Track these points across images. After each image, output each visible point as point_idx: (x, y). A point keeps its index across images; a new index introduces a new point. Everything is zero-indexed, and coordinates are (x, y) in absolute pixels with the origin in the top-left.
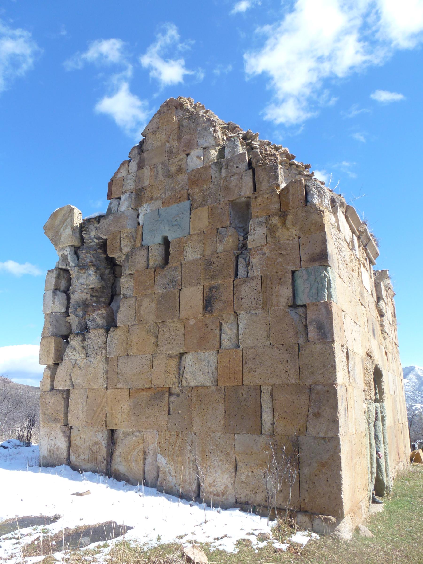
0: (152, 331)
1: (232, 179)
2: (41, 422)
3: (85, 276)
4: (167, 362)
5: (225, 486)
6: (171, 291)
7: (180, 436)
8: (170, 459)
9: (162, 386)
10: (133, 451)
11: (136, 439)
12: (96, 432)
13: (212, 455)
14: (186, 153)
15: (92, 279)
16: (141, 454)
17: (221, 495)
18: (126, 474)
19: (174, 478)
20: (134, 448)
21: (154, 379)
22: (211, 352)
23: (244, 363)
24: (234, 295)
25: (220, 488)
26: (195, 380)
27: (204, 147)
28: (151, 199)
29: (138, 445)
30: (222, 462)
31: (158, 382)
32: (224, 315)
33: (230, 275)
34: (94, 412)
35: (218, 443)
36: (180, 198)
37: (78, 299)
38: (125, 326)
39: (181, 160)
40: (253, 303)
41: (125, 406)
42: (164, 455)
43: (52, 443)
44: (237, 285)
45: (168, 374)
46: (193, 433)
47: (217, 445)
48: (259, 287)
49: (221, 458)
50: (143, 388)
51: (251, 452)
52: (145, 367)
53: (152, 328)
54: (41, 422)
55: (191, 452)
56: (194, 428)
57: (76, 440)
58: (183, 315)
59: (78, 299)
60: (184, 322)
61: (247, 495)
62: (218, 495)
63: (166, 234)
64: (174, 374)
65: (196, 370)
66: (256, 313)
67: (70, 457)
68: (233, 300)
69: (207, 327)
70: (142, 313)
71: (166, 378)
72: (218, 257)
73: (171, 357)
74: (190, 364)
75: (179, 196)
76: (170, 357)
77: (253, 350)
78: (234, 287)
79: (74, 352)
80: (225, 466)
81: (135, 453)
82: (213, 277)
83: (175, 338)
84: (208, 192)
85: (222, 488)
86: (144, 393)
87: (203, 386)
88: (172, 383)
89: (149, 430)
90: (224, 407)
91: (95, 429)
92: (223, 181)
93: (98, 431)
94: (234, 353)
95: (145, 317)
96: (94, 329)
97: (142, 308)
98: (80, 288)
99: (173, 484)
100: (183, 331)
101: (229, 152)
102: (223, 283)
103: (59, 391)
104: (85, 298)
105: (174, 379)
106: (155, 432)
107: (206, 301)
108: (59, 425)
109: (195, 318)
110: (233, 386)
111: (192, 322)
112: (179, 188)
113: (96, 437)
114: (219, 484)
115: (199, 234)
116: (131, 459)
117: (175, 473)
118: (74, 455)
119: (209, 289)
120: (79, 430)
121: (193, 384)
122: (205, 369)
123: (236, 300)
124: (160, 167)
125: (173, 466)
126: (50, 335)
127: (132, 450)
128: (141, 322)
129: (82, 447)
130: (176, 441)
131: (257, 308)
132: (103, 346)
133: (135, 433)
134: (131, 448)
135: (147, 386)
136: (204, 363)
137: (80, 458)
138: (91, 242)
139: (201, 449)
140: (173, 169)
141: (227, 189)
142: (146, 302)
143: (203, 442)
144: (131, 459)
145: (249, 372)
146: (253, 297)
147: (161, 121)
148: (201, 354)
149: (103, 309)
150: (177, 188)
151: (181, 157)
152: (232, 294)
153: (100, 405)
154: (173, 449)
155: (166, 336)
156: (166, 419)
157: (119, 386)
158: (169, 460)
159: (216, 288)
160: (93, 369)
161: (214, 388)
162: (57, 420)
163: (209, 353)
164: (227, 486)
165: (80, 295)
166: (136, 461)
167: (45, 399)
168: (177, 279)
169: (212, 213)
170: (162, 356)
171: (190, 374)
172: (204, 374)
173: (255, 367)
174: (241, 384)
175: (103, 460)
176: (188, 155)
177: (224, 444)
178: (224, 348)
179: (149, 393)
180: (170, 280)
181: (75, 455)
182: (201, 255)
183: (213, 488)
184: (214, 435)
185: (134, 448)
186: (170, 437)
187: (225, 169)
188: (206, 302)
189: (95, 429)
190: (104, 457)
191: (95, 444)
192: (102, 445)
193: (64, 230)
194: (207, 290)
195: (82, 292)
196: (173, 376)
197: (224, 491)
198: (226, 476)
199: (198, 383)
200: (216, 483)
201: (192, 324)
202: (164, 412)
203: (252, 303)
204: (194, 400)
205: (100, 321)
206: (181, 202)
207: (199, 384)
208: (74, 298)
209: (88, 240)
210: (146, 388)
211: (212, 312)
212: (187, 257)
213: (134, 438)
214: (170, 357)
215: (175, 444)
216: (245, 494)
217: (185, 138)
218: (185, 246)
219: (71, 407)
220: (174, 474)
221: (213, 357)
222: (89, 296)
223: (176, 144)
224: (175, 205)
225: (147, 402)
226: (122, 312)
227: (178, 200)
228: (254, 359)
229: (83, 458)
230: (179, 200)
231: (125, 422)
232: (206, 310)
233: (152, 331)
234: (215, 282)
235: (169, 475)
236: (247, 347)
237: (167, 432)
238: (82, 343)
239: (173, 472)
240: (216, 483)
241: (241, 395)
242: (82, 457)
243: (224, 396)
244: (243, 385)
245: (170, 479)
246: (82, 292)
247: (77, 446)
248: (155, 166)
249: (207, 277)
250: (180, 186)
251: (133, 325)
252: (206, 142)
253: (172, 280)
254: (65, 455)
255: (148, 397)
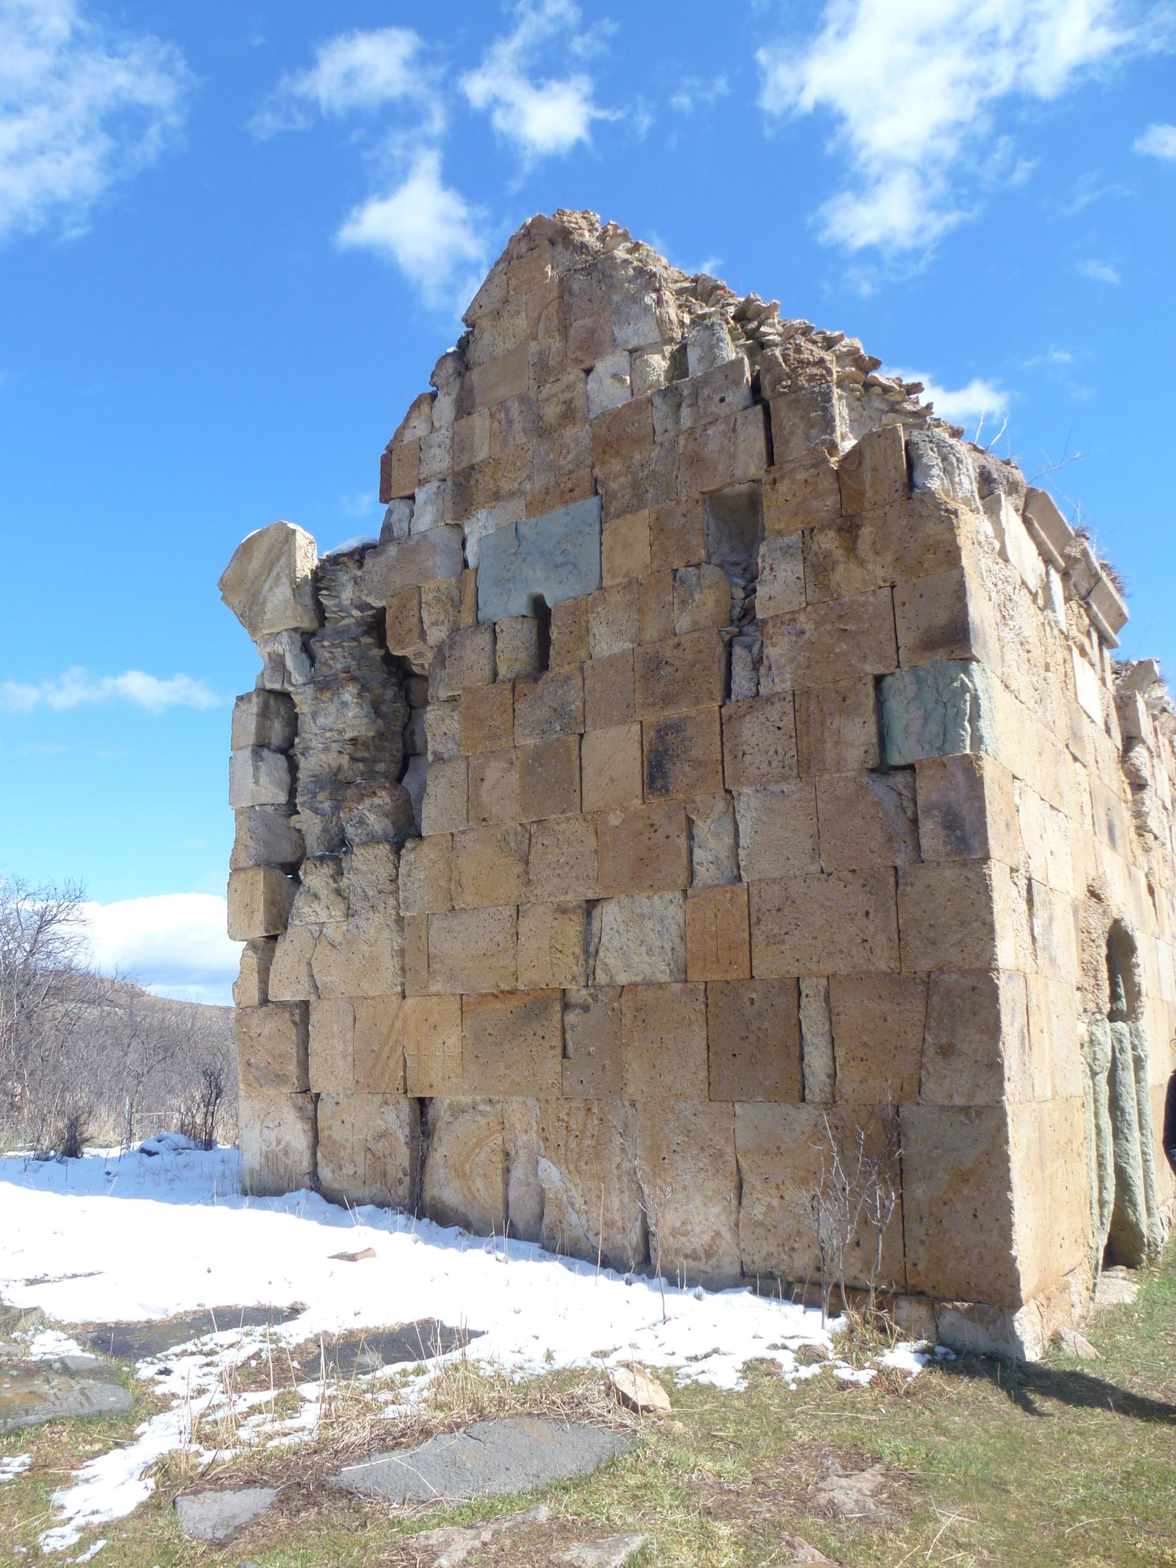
0: (513, 844)
1: (709, 432)
2: (242, 1086)
3: (332, 708)
4: (555, 923)
5: (713, 1234)
6: (558, 740)
7: (595, 1110)
8: (572, 1168)
9: (544, 986)
10: (477, 1151)
11: (483, 1121)
12: (381, 1106)
13: (677, 1157)
14: (584, 366)
15: (350, 714)
16: (498, 1158)
17: (703, 1255)
18: (462, 1209)
19: (584, 1218)
20: (479, 1143)
21: (523, 969)
22: (668, 896)
23: (754, 920)
24: (722, 743)
25: (700, 1239)
26: (628, 967)
27: (630, 347)
28: (497, 496)
29: (487, 1137)
30: (703, 1175)
31: (534, 977)
32: (698, 799)
33: (711, 693)
34: (373, 1056)
35: (692, 1127)
36: (571, 491)
37: (318, 767)
38: (444, 835)
39: (570, 387)
40: (774, 764)
41: (452, 1038)
42: (554, 1159)
43: (272, 1136)
44: (730, 718)
45: (559, 955)
46: (627, 1103)
47: (689, 1131)
48: (788, 723)
49: (701, 1165)
50: (495, 992)
51: (778, 1148)
52: (499, 938)
53: (511, 838)
54: (242, 1086)
55: (623, 1150)
56: (631, 1089)
57: (330, 1128)
58: (592, 800)
59: (318, 767)
60: (597, 820)
61: (770, 1255)
62: (694, 1256)
63: (538, 590)
64: (573, 954)
65: (629, 943)
66: (783, 792)
67: (319, 1169)
68: (719, 758)
69: (656, 831)
70: (485, 799)
71: (552, 964)
72: (679, 645)
73: (564, 912)
74: (615, 927)
75: (569, 485)
76: (562, 910)
77: (776, 887)
78: (722, 724)
79: (315, 906)
80: (711, 1185)
81: (482, 1156)
82: (667, 700)
83: (572, 862)
84: (646, 472)
85: (707, 1238)
86: (498, 1005)
87: (650, 984)
88: (569, 977)
89: (514, 1099)
90: (704, 1034)
91: (378, 1099)
92: (686, 440)
93: (386, 1103)
94: (728, 896)
95: (494, 810)
96: (364, 844)
97: (485, 786)
98: (322, 740)
99: (579, 1232)
100: (592, 842)
101: (700, 360)
102: (693, 713)
103: (282, 1005)
104: (334, 765)
105: (574, 968)
106: (531, 1102)
107: (649, 762)
108: (287, 1090)
109: (624, 809)
110: (728, 982)
111: (614, 820)
112: (569, 463)
113: (382, 1119)
114: (697, 1230)
115: (627, 586)
116: (471, 1172)
117: (586, 1203)
118: (327, 1166)
119: (658, 731)
120: (337, 1103)
121: (622, 979)
122: (654, 939)
123: (728, 758)
124: (515, 408)
125: (580, 1188)
126: (251, 863)
127: (474, 1149)
128: (484, 823)
129: (348, 1145)
130: (585, 1125)
131: (785, 778)
132: (390, 887)
133: (481, 1107)
134: (470, 1144)
135: (505, 987)
136: (649, 924)
137: (344, 1171)
138: (343, 618)
139: (648, 1143)
140: (551, 412)
141: (696, 461)
142: (492, 773)
143: (654, 1126)
144: (471, 1172)
145: (767, 945)
146: (773, 749)
147: (513, 282)
148: (643, 902)
149: (384, 794)
150: (562, 462)
151: (572, 378)
152: (719, 743)
153: (389, 1037)
154: (578, 1145)
155: (550, 856)
156: (558, 1068)
157: (436, 987)
158: (570, 1172)
159: (676, 727)
160: (365, 948)
161: (677, 987)
162: (280, 1079)
163: (661, 897)
164: (718, 1234)
165: (323, 757)
166: (485, 1175)
167: (247, 1027)
168: (573, 707)
169: (659, 528)
170: (541, 909)
171: (615, 954)
172: (649, 952)
173: (783, 932)
174: (748, 976)
175: (400, 1175)
176: (588, 371)
177: (707, 1130)
178: (700, 884)
179: (513, 1003)
180: (555, 710)
181: (331, 1166)
182: (632, 641)
183: (683, 1239)
184: (681, 1105)
185: (479, 1143)
186: (568, 1114)
187: (690, 406)
188: (651, 766)
189: (378, 1099)
190: (404, 1169)
191: (381, 1137)
192: (397, 1139)
193: (271, 589)
194: (653, 733)
195: (326, 750)
196: (571, 959)
197: (710, 1246)
198: (716, 1210)
199: (637, 975)
200: (689, 1227)
201: (616, 823)
202: (551, 1052)
203: (770, 763)
204: (627, 1021)
205: (377, 823)
206: (574, 500)
207: (638, 979)
208: (308, 765)
209: (335, 613)
210: (502, 992)
211: (667, 791)
212: (598, 649)
213: (479, 1118)
214: (562, 910)
215: (583, 1132)
216: (764, 1253)
217: (580, 324)
218: (591, 620)
219: (313, 1045)
220: (584, 1207)
221: (672, 907)
222: (345, 761)
223: (556, 344)
224: (561, 510)
225: (507, 1029)
226: (433, 798)
227: (568, 496)
228: (779, 910)
229: (351, 1172)
230: (568, 495)
231: (454, 1080)
232: (650, 788)
233: (513, 844)
234: (671, 714)
235: (570, 1210)
236: (760, 880)
237: (562, 1101)
238: (335, 881)
239: (579, 1202)
240: (689, 1227)
241: (748, 1003)
242: (349, 1170)
243: (703, 1007)
244: (752, 977)
245: (573, 1218)
246: (326, 750)
247: (335, 1142)
248: (503, 405)
249: (651, 700)
250: (570, 457)
251: (463, 832)
252: (636, 333)
253: (561, 712)
254: (306, 1165)
255: (510, 1015)
